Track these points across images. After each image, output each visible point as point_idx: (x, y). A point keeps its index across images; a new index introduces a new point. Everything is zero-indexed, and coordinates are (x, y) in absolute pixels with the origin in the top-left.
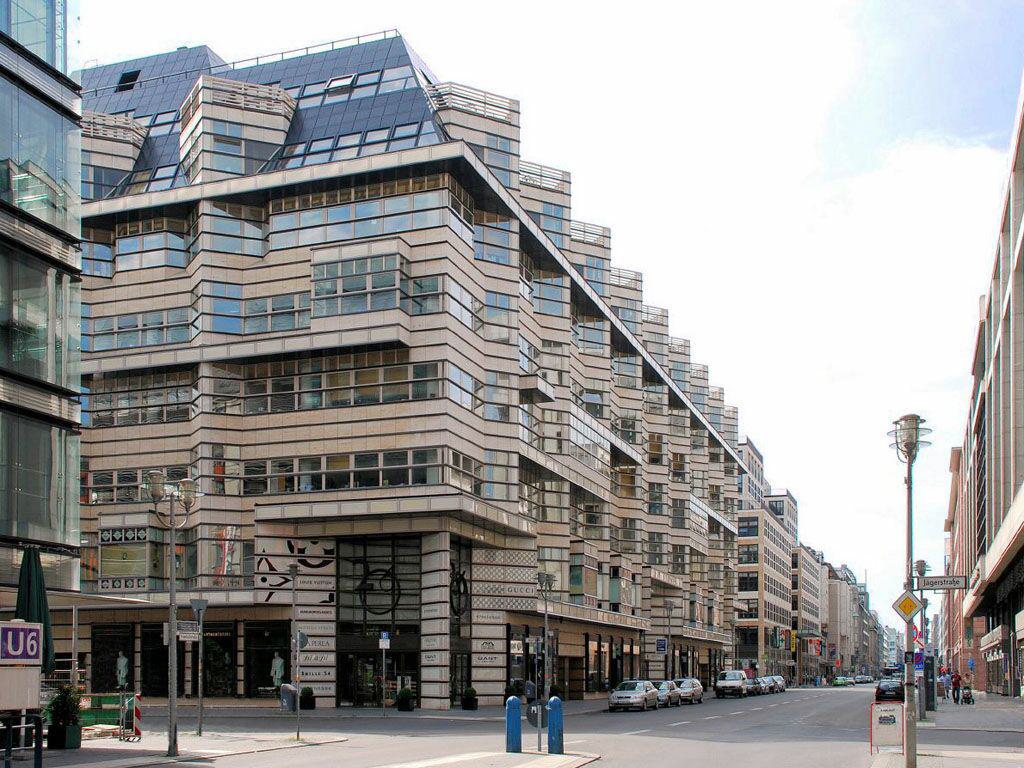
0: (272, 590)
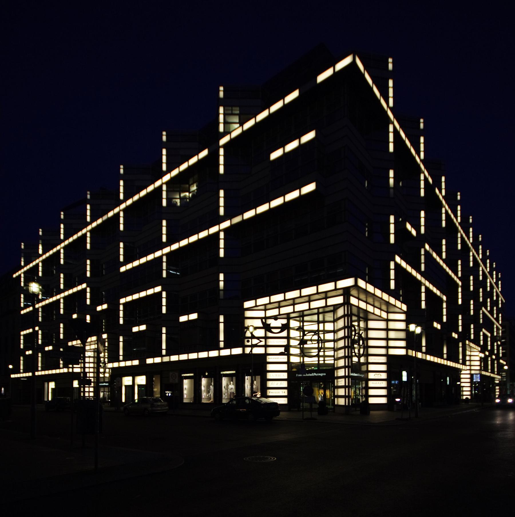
0: (253, 346)
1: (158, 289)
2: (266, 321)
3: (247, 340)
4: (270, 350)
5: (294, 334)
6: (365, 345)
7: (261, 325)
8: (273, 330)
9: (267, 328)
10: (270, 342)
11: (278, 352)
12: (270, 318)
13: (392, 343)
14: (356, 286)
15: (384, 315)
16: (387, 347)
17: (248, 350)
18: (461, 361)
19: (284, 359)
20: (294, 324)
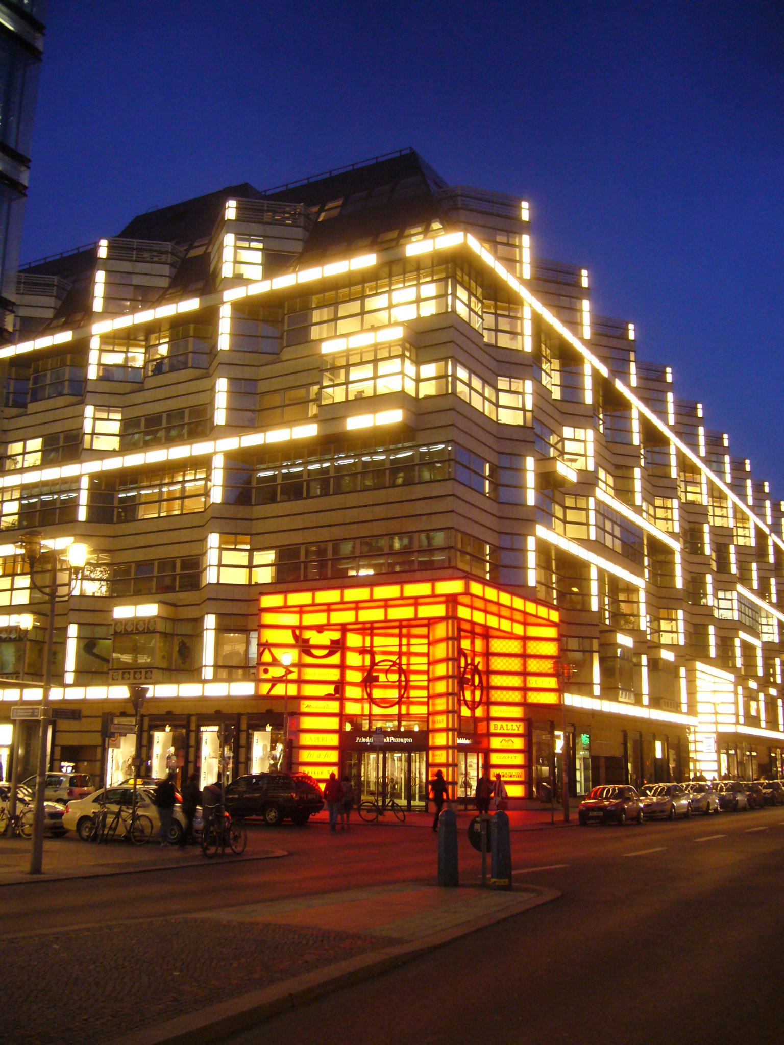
0: (275, 681)
2: (301, 633)
3: (263, 668)
4: (308, 690)
5: (353, 659)
6: (485, 684)
7: (292, 641)
8: (315, 652)
9: (305, 647)
10: (310, 674)
11: (322, 694)
13: (533, 682)
14: (467, 593)
15: (519, 629)
16: (525, 689)
17: (265, 688)
18: (684, 708)
19: (334, 706)
20: (354, 640)
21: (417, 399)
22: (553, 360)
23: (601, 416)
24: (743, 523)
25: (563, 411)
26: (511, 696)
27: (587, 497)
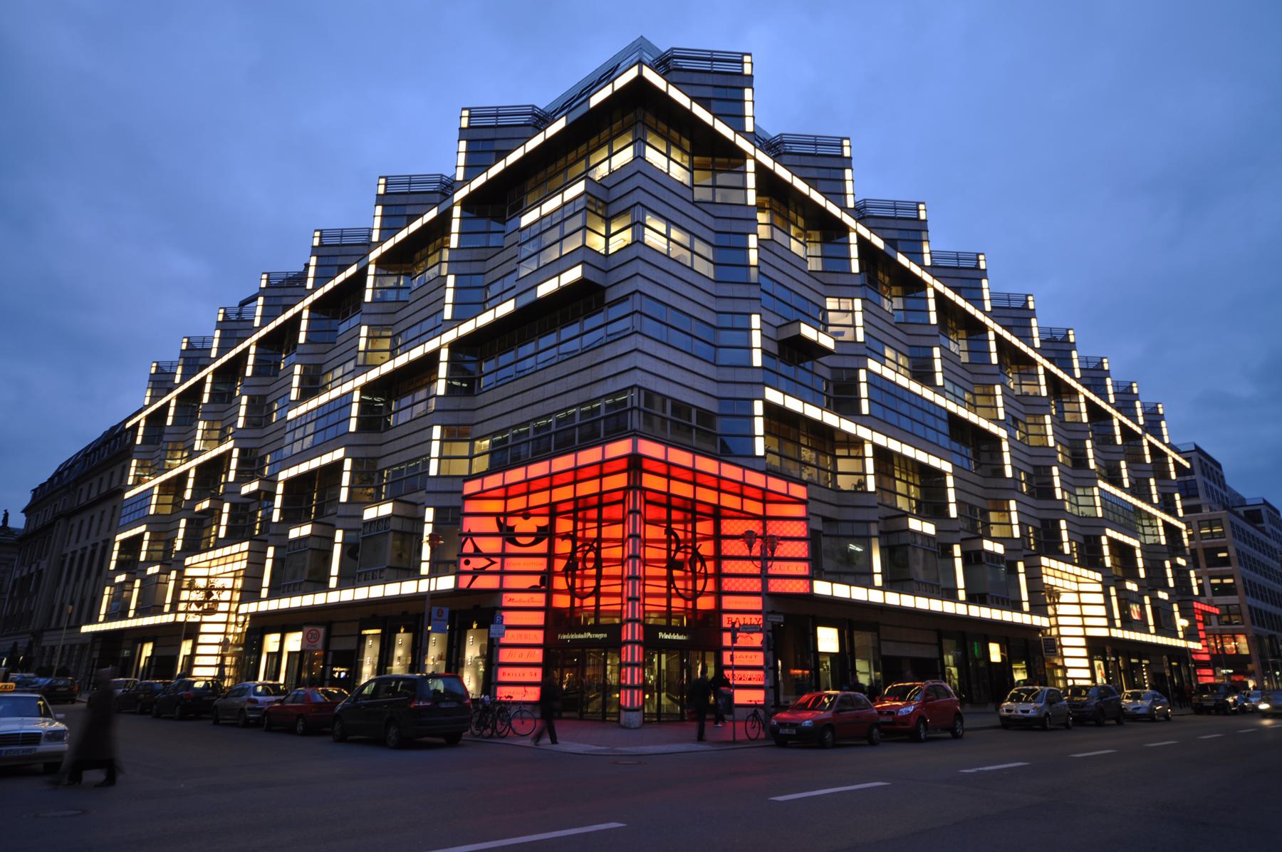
0: (476, 573)
1: (339, 454)
2: (505, 520)
4: (512, 582)
8: (520, 540)
9: (508, 534)
10: (514, 564)
12: (514, 514)
15: (754, 507)
17: (465, 581)
19: (539, 600)
21: (607, 255)
22: (959, 331)
23: (1053, 402)
24: (1070, 398)
25: (716, 215)
26: (748, 585)
27: (1093, 487)
